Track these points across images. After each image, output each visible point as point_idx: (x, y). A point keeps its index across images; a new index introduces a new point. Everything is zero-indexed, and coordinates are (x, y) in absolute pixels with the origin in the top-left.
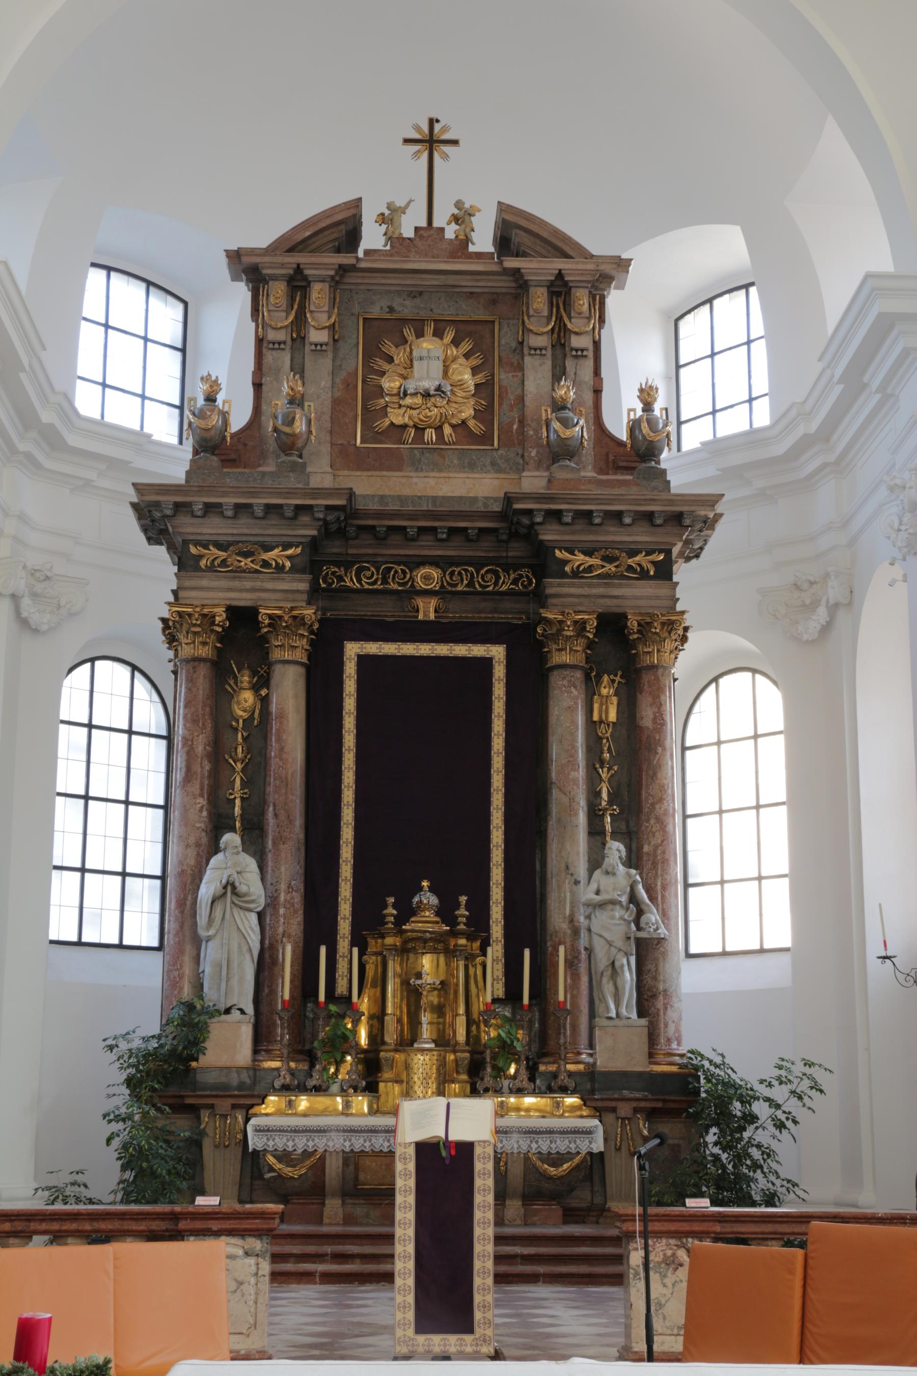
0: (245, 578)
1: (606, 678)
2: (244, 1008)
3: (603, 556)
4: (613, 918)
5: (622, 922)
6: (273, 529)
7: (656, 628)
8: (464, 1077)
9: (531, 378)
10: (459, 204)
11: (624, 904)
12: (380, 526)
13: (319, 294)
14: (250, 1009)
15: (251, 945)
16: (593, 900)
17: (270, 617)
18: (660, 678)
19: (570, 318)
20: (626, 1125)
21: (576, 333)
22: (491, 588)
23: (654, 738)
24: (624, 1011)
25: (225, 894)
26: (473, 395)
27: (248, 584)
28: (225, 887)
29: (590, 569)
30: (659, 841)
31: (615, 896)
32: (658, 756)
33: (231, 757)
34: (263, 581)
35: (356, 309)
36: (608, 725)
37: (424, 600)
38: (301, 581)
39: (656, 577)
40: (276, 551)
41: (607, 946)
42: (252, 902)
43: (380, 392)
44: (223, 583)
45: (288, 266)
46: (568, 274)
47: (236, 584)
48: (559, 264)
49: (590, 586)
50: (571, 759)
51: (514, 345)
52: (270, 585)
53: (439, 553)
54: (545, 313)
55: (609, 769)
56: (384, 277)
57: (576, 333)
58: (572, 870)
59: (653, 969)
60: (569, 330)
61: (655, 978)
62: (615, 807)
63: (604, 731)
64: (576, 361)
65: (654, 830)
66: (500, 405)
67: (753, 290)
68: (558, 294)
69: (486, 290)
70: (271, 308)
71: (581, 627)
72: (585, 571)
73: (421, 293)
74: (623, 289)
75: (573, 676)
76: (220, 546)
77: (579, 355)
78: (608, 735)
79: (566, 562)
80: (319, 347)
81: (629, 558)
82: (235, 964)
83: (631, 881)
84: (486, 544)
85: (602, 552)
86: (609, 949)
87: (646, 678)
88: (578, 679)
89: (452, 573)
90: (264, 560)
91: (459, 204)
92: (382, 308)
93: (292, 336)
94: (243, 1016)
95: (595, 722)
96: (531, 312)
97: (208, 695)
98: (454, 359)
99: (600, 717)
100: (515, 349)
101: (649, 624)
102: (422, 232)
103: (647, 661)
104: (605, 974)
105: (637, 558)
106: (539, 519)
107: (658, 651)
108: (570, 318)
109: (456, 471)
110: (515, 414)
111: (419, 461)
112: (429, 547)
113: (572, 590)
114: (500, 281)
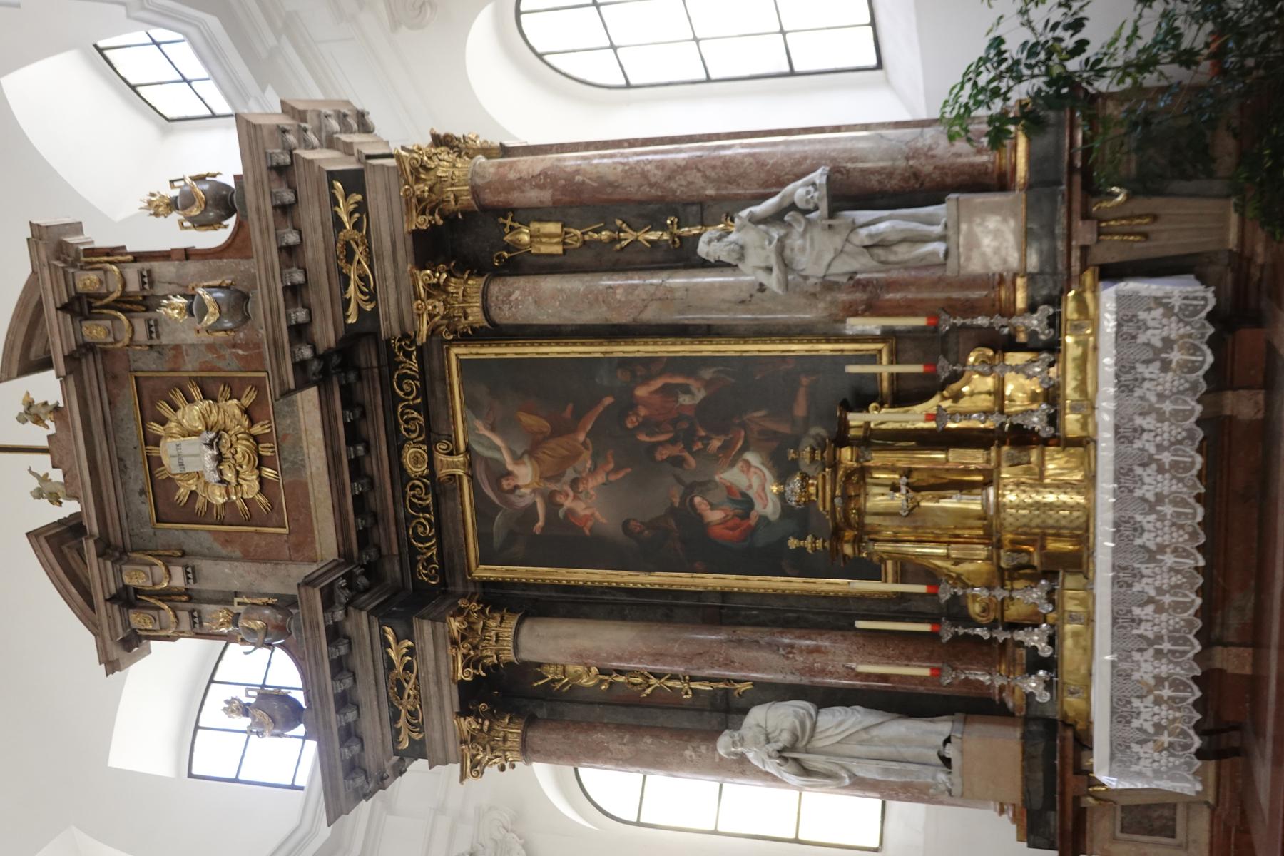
0: (425, 694)
1: (508, 238)
2: (943, 738)
3: (347, 262)
4: (803, 249)
5: (808, 236)
6: (364, 662)
7: (424, 192)
8: (1034, 455)
9: (183, 335)
10: (21, 419)
11: (782, 232)
12: (357, 526)
13: (136, 577)
14: (943, 727)
15: (860, 727)
16: (778, 279)
17: (465, 666)
18: (487, 180)
19: (107, 296)
20: (1108, 226)
21: (124, 285)
22: (418, 384)
23: (564, 186)
24: (937, 229)
25: (795, 760)
26: (215, 400)
27: (433, 689)
28: (786, 759)
29: (364, 279)
30: (699, 175)
31: (771, 249)
32: (587, 181)
33: (644, 690)
34: (427, 673)
35: (150, 531)
36: (566, 233)
37: (439, 468)
38: (421, 630)
39: (362, 191)
40: (393, 654)
41: (844, 256)
42: (803, 724)
43: (229, 505)
44: (435, 715)
45: (110, 611)
46: (60, 299)
47: (434, 702)
48: (50, 311)
49: (384, 279)
50: (601, 299)
51: (154, 354)
52: (431, 665)
53: (384, 448)
54: (108, 323)
55: (621, 230)
56: (109, 504)
57: (124, 285)
58: (745, 295)
59: (877, 177)
60: (122, 296)
61: (890, 174)
62: (669, 222)
63: (575, 238)
64: (156, 283)
65: (684, 183)
66: (220, 370)
67: (101, 44)
68: (90, 307)
69: (103, 386)
70: (157, 627)
71: (435, 290)
72: (367, 285)
73: (120, 459)
74: (80, 223)
75: (497, 297)
76: (395, 717)
77: (147, 279)
78: (578, 232)
79: (360, 310)
80: (190, 576)
81: (345, 228)
82: (885, 751)
83: (750, 224)
84: (366, 395)
85: (342, 264)
86: (848, 254)
87: (489, 197)
88: (500, 289)
89: (407, 430)
90: (404, 670)
91: (21, 419)
92: (143, 503)
93: (185, 602)
94: (953, 740)
95: (564, 251)
96: (110, 339)
97: (564, 737)
98: (180, 424)
99: (557, 243)
100: (159, 352)
101: (420, 200)
102: (56, 461)
103: (467, 198)
104: (883, 258)
105: (345, 218)
106: (307, 352)
107: (452, 185)
108: (109, 293)
109: (299, 421)
110: (227, 352)
111: (294, 463)
112: (379, 461)
113: (392, 300)
114: (89, 374)
